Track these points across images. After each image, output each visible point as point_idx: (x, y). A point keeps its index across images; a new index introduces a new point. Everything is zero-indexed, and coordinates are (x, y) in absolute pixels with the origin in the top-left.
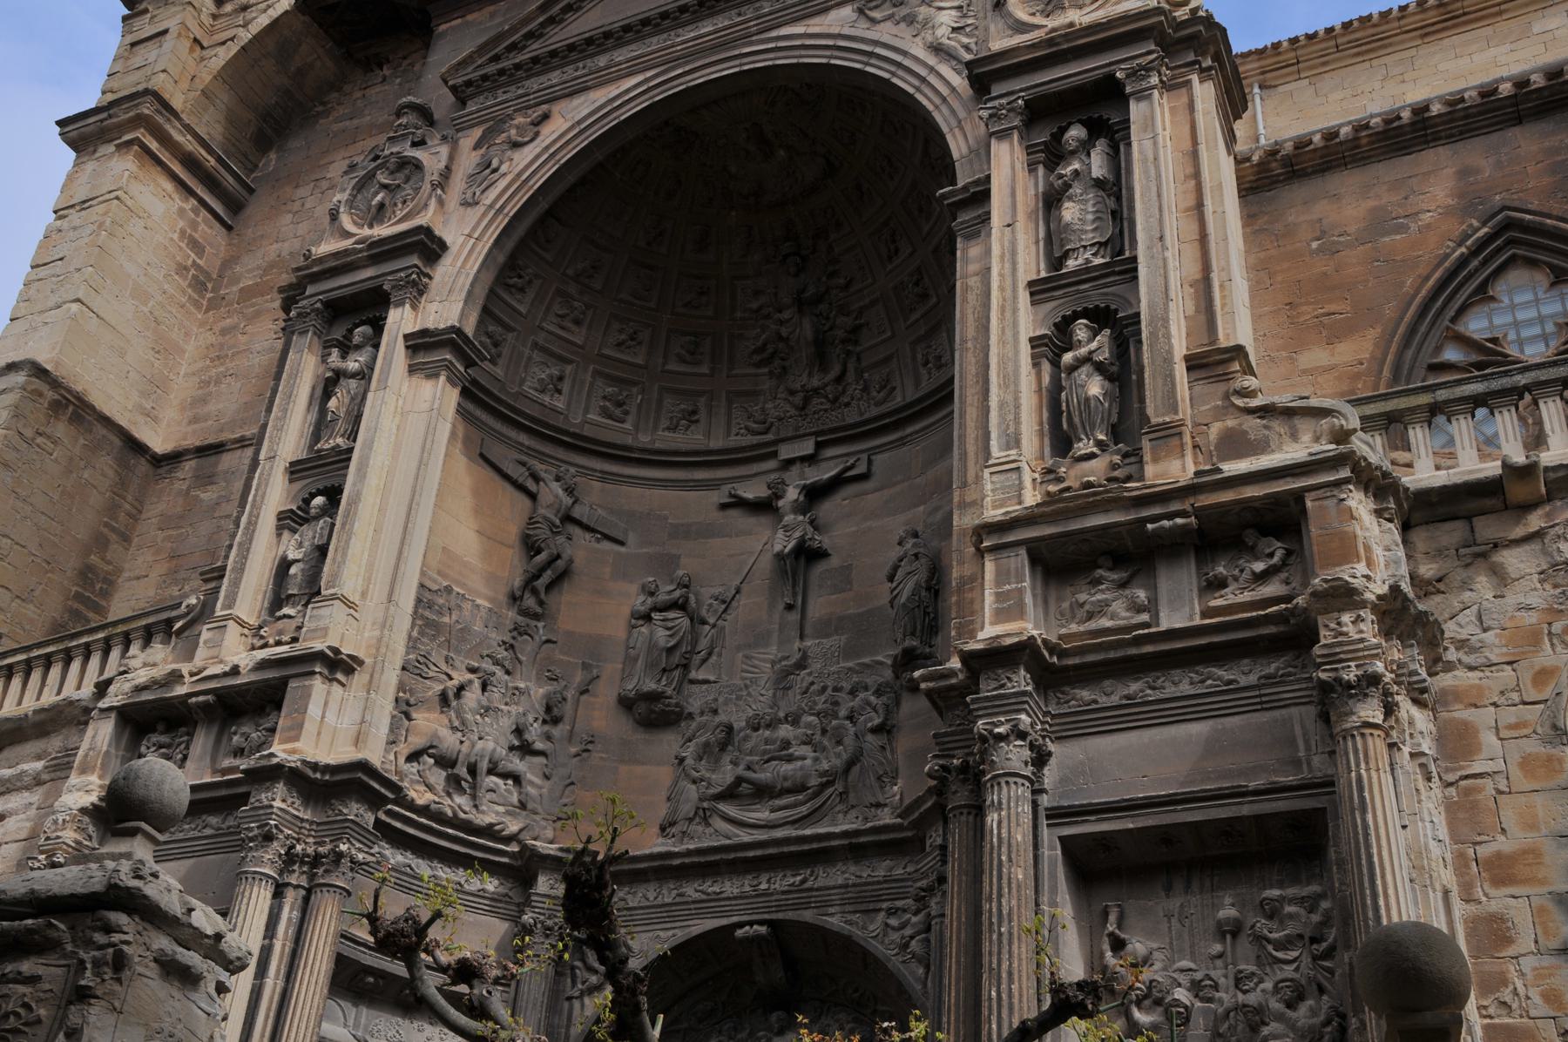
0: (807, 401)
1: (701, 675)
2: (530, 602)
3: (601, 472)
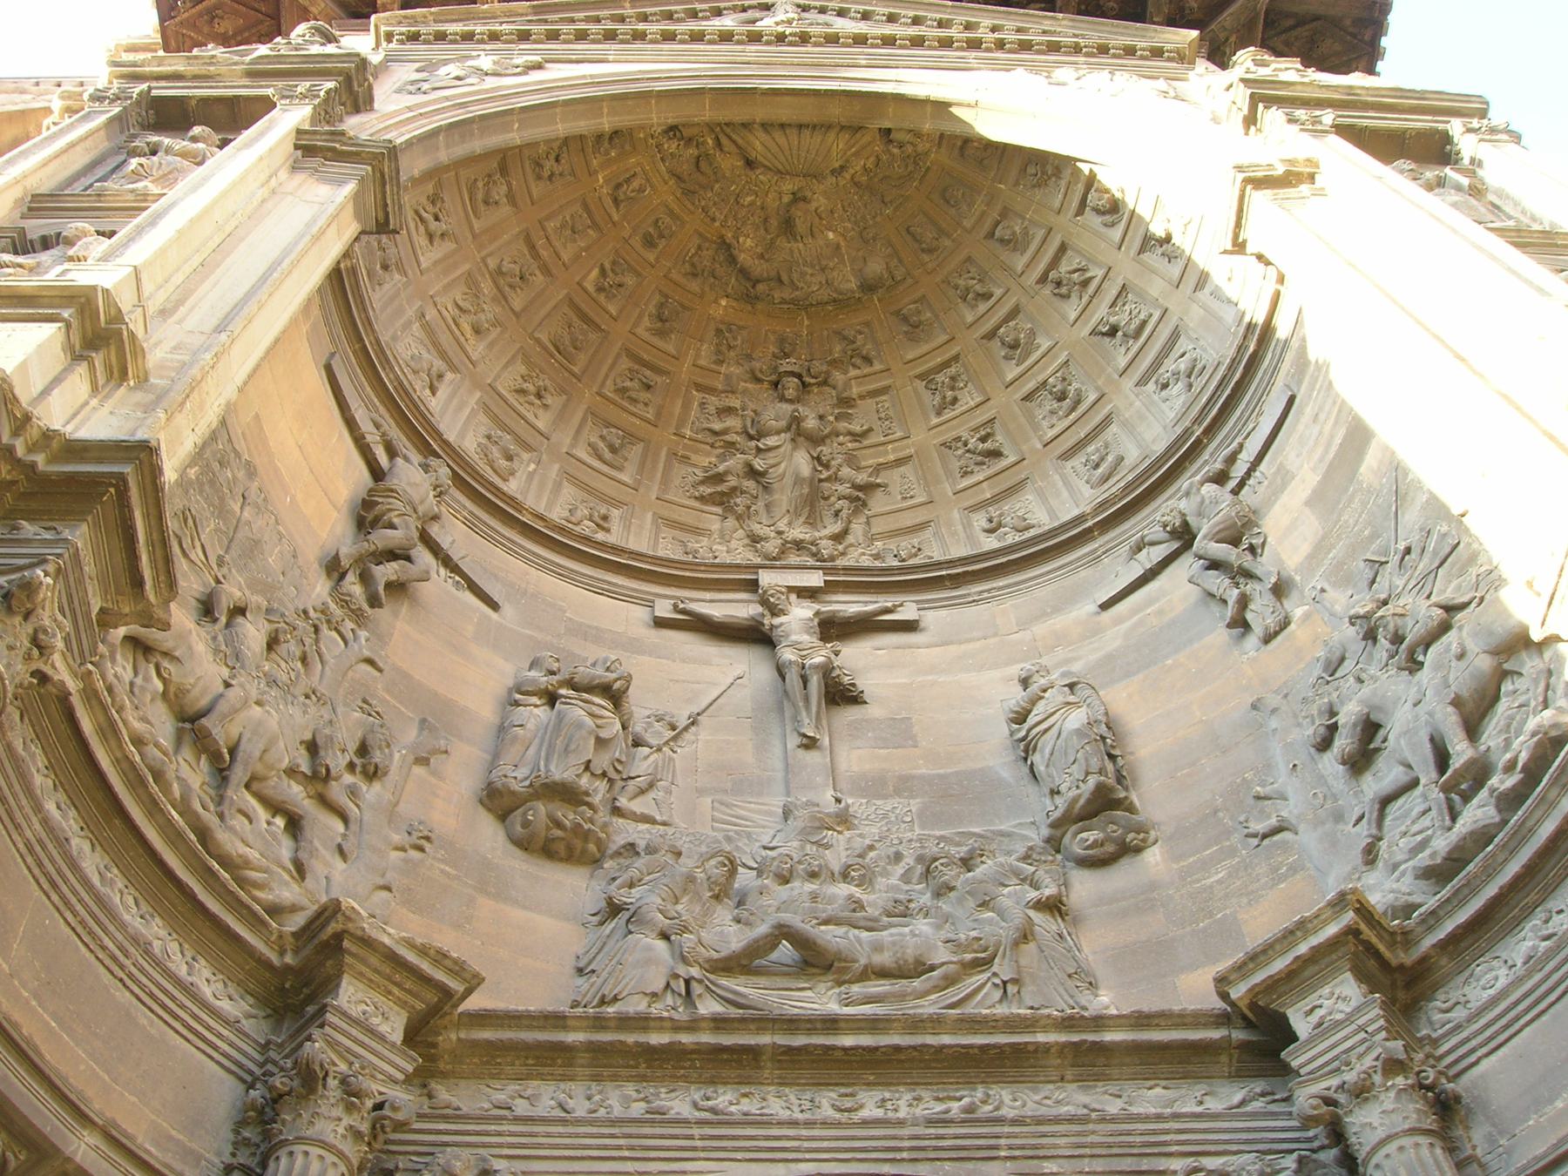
0: (783, 552)
1: (637, 806)
2: (353, 586)
3: (471, 513)
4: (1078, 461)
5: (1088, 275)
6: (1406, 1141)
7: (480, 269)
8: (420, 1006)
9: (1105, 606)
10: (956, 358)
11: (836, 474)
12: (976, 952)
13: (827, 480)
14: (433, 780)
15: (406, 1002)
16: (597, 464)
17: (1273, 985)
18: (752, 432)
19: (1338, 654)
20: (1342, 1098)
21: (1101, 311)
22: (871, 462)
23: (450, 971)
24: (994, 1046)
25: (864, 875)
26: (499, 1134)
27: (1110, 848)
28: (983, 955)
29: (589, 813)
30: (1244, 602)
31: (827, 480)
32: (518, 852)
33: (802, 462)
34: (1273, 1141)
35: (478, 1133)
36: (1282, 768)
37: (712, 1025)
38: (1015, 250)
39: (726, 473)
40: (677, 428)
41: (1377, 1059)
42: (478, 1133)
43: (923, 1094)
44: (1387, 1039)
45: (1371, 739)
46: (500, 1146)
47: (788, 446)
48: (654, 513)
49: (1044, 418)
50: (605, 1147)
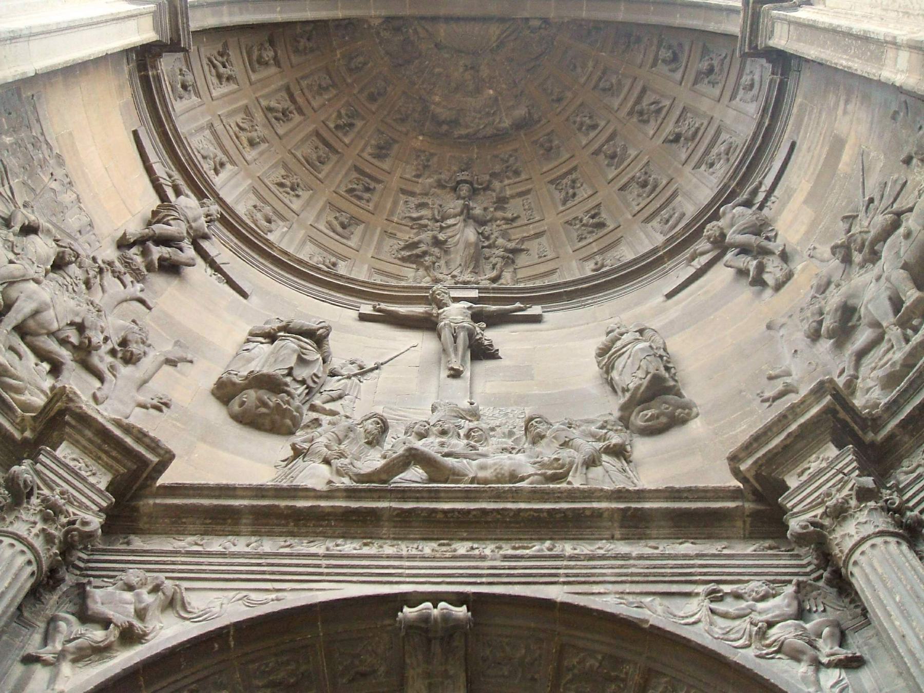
4: (655, 223)
5: (660, 105)
6: (879, 541)
7: (255, 105)
8: (122, 470)
9: (669, 296)
10: (575, 169)
11: (494, 242)
12: (556, 469)
13: (489, 247)
14: (178, 375)
15: (112, 467)
16: (332, 234)
17: (773, 459)
18: (438, 218)
19: (825, 280)
20: (827, 522)
21: (669, 128)
22: (517, 236)
23: (148, 447)
24: (559, 511)
25: (481, 435)
26: (173, 563)
27: (663, 420)
28: (561, 471)
29: (287, 398)
30: (761, 268)
31: (489, 247)
32: (234, 424)
33: (471, 234)
34: (777, 574)
35: (157, 563)
36: (787, 354)
37: (345, 494)
38: (613, 95)
39: (420, 242)
40: (388, 215)
41: (851, 489)
42: (157, 563)
43: (504, 546)
44: (858, 476)
45: (849, 319)
46: (173, 571)
47: (461, 225)
48: (369, 265)
49: (633, 200)
50: (253, 572)
